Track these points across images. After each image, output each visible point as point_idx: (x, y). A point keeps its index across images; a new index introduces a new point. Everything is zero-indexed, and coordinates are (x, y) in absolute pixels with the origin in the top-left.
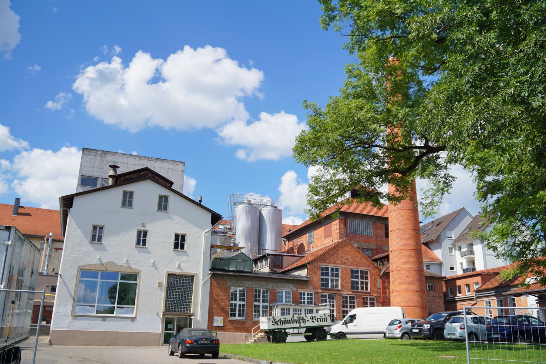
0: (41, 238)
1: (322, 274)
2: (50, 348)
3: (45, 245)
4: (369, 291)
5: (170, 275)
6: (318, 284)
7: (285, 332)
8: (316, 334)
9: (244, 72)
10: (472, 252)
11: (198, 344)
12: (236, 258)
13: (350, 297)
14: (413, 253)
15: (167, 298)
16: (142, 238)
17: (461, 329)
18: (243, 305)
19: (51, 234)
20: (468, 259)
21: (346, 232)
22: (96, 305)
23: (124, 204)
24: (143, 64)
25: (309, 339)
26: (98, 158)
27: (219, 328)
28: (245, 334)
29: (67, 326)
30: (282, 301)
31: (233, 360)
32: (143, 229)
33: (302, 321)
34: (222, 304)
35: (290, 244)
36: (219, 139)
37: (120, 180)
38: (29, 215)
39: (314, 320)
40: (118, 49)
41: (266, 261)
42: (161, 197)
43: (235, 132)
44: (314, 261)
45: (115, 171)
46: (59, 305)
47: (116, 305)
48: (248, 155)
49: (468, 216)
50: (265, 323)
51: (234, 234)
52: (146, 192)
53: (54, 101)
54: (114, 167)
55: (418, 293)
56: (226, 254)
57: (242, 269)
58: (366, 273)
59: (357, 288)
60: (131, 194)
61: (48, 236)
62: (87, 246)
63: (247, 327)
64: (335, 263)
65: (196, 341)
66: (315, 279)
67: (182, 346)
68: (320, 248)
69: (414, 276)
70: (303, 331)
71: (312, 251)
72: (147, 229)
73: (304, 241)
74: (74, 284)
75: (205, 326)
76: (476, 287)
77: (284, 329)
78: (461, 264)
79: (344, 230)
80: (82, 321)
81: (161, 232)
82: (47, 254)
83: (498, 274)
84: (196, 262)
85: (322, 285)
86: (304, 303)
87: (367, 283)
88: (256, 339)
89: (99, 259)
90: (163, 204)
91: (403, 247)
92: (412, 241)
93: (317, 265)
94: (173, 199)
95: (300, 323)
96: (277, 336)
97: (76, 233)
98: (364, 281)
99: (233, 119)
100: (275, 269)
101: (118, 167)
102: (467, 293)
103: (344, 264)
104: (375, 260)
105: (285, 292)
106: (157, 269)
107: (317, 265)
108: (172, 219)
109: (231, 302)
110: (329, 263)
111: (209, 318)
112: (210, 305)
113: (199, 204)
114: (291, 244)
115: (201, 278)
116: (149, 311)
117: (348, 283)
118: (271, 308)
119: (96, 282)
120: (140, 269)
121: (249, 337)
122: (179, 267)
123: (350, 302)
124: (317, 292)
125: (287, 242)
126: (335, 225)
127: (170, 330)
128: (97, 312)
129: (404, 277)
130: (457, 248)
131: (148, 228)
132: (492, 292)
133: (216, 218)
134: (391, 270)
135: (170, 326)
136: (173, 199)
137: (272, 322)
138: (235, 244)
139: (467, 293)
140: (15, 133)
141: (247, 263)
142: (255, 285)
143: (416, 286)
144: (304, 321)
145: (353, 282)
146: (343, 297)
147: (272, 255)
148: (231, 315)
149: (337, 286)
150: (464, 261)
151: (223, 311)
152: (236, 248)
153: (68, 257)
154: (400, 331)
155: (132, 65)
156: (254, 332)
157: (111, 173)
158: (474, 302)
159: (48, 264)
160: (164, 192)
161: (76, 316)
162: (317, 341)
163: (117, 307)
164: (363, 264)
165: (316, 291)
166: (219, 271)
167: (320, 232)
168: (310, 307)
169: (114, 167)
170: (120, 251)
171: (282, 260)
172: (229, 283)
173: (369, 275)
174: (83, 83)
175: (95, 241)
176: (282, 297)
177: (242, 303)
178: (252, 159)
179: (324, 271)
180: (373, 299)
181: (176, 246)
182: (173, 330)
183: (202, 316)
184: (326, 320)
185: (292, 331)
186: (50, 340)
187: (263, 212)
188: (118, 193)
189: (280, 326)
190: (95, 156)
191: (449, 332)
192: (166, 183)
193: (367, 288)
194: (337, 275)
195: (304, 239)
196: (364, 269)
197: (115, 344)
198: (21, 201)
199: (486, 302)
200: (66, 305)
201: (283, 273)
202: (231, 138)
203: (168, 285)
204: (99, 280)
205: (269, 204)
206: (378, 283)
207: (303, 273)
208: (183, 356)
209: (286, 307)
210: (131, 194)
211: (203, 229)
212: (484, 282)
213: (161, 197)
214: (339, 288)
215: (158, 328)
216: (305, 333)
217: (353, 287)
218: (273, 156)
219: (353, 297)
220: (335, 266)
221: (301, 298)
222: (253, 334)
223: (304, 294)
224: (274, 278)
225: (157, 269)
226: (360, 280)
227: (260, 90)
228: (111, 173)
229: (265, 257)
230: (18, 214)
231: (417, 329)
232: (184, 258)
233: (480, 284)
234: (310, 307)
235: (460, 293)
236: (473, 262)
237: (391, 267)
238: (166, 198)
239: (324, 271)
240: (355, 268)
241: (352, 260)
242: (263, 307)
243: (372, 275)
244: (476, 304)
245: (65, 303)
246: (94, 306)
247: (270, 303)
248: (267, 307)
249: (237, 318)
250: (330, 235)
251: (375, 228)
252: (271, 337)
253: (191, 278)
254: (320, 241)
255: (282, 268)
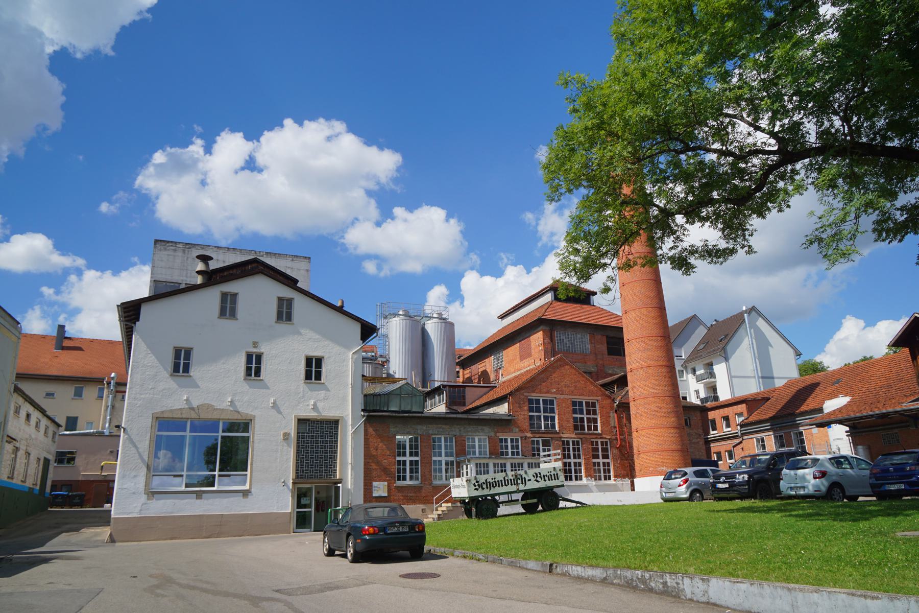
0: (99, 381)
1: (531, 410)
2: (109, 550)
3: (105, 390)
4: (599, 431)
5: (301, 421)
6: (526, 425)
7: (495, 500)
8: (543, 500)
9: (373, 151)
10: (712, 375)
11: (386, 534)
12: (398, 392)
13: (573, 442)
14: (664, 370)
15: (298, 456)
16: (254, 366)
17: (815, 478)
18: (417, 462)
19: (113, 375)
20: (705, 384)
21: (554, 349)
22: (184, 473)
23: (223, 313)
24: (231, 147)
25: (530, 509)
26: (180, 254)
27: (380, 499)
28: (422, 506)
29: (137, 510)
30: (474, 453)
31: (451, 561)
32: (255, 350)
33: (519, 482)
34: (385, 462)
35: (465, 372)
36: (339, 249)
37: (213, 277)
38: (79, 349)
39: (539, 479)
40: (198, 129)
41: (439, 395)
42: (280, 300)
43: (363, 237)
44: (518, 390)
45: (207, 264)
46: (123, 477)
47: (216, 473)
48: (379, 268)
49: (701, 327)
50: (460, 489)
51: (388, 361)
52: (257, 294)
53: (111, 203)
54: (205, 259)
55: (676, 430)
56: (378, 389)
57: (408, 408)
58: (594, 405)
59: (583, 428)
60: (234, 296)
61: (109, 377)
62: (167, 382)
63: (424, 495)
64: (548, 392)
65: (383, 529)
66: (521, 418)
67: (355, 539)
68: (513, 375)
69: (667, 406)
70: (519, 496)
71: (502, 380)
72: (262, 351)
73: (488, 366)
74: (148, 442)
75: (359, 499)
76: (739, 420)
77: (493, 496)
78: (697, 392)
79: (549, 346)
80: (168, 501)
81: (285, 354)
82: (109, 404)
83: (768, 399)
84: (340, 400)
85: (532, 425)
86: (507, 454)
87: (595, 421)
88: (440, 513)
89: (186, 400)
90: (285, 312)
91: (648, 363)
92: (660, 353)
93: (522, 397)
94: (301, 305)
95: (518, 484)
96: (481, 508)
97: (146, 368)
98: (592, 416)
99: (357, 219)
100: (455, 408)
101: (211, 258)
102: (725, 430)
103: (559, 392)
104: (603, 386)
105: (479, 441)
106: (280, 412)
107: (522, 397)
108: (300, 334)
109: (398, 458)
110: (540, 392)
111: (365, 485)
112: (366, 464)
113: (340, 310)
114: (467, 373)
115: (350, 422)
116: (270, 481)
117: (568, 421)
118: (459, 465)
119: (183, 437)
120: (253, 413)
121: (428, 511)
122: (315, 407)
123: (574, 449)
124: (526, 437)
125: (461, 371)
126: (537, 339)
127: (305, 506)
128: (186, 486)
129: (653, 407)
130: (689, 370)
131: (263, 349)
132: (767, 426)
133: (368, 331)
134: (631, 399)
135: (304, 501)
136: (301, 305)
137: (475, 485)
138: (388, 374)
139: (725, 430)
140: (61, 247)
141: (414, 399)
142: (432, 430)
143: (672, 420)
144: (524, 482)
145: (575, 419)
146: (563, 442)
147: (450, 386)
148: (399, 479)
149: (553, 426)
150: (701, 387)
151: (385, 474)
152: (390, 379)
153: (135, 399)
154: (687, 488)
155: (216, 148)
156: (437, 503)
157: (200, 266)
158: (738, 441)
159: (110, 419)
160: (286, 292)
161: (152, 494)
162: (544, 510)
163: (220, 476)
164: (589, 393)
165: (523, 435)
166: (378, 412)
167: (511, 352)
168: (518, 459)
169: (205, 259)
170: (218, 388)
171: (464, 392)
172: (393, 429)
173: (598, 408)
174: (147, 181)
175: (178, 372)
176: (474, 447)
177: (414, 458)
178: (385, 272)
179: (533, 405)
180: (606, 443)
181: (308, 376)
182: (311, 507)
183: (355, 483)
184: (556, 477)
185: (503, 498)
186: (111, 535)
187: (427, 327)
188: (213, 296)
189: (486, 492)
190: (175, 250)
191: (793, 485)
192: (290, 282)
193: (596, 428)
194: (552, 411)
195: (489, 364)
196: (591, 399)
197: (218, 535)
198: (66, 329)
199: (758, 441)
200: (135, 476)
201: (467, 412)
202: (356, 248)
203: (298, 437)
204: (188, 434)
205: (435, 315)
206: (612, 419)
207: (503, 409)
208: (359, 558)
209: (482, 461)
210: (234, 296)
211: (348, 348)
212: (750, 412)
213: (280, 300)
214: (557, 429)
215: (286, 504)
216: (522, 499)
217: (576, 428)
218: (413, 267)
219: (578, 442)
220: (548, 397)
221: (502, 447)
222: (435, 506)
223: (506, 440)
224: (461, 419)
225: (280, 412)
226: (585, 417)
227: (395, 180)
228: (200, 266)
229: (438, 391)
230: (63, 348)
231: (724, 482)
232: (322, 393)
233: (746, 415)
234: (518, 459)
235: (714, 429)
236: (714, 389)
237: (630, 394)
238: (290, 302)
239: (533, 405)
240: (577, 398)
241: (571, 386)
242: (447, 464)
243: (602, 408)
244: (741, 442)
245: (133, 474)
246: (182, 476)
247: (457, 456)
248: (452, 462)
249: (408, 482)
250: (529, 355)
251: (593, 341)
252: (474, 510)
253: (334, 424)
254: (513, 366)
255: (464, 405)
